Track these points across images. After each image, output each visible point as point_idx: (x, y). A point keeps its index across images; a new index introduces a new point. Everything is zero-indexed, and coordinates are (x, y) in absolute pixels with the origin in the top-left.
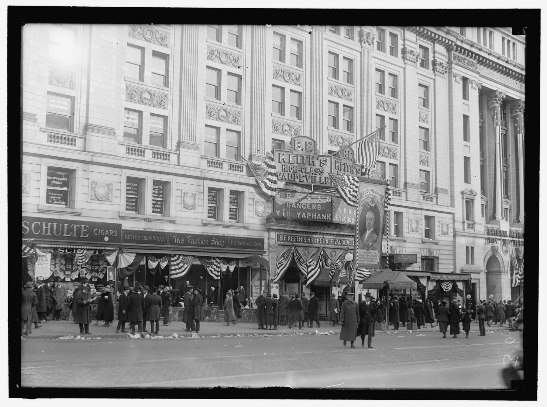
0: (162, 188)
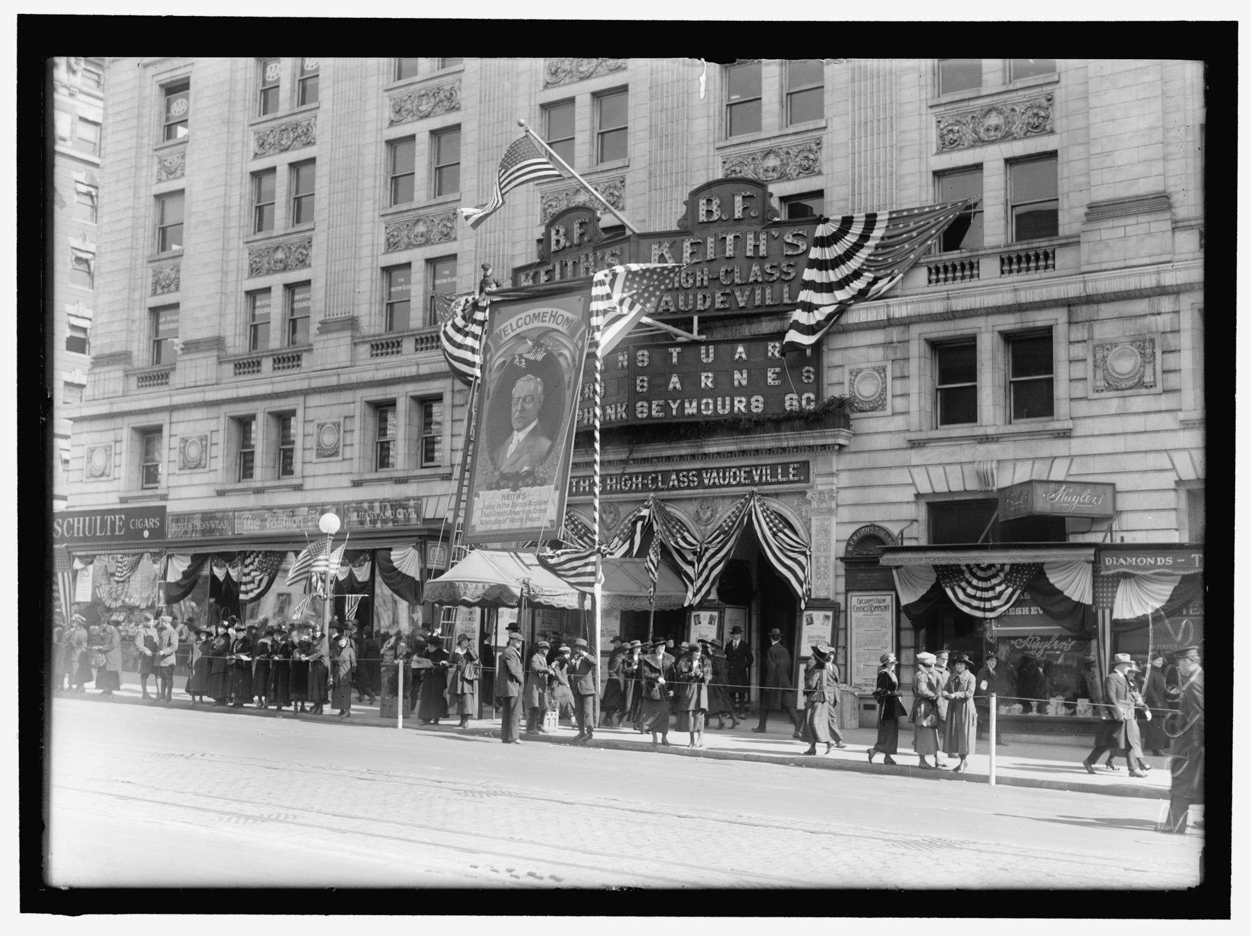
0: (956, 405)
